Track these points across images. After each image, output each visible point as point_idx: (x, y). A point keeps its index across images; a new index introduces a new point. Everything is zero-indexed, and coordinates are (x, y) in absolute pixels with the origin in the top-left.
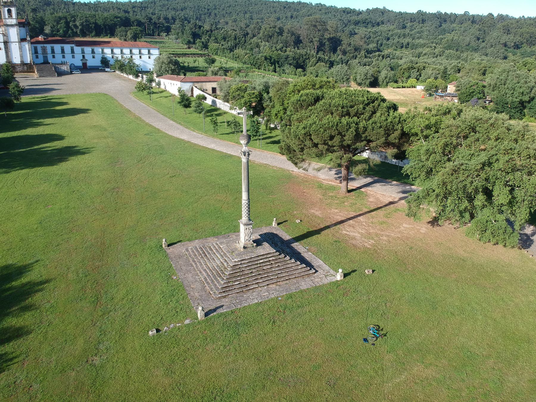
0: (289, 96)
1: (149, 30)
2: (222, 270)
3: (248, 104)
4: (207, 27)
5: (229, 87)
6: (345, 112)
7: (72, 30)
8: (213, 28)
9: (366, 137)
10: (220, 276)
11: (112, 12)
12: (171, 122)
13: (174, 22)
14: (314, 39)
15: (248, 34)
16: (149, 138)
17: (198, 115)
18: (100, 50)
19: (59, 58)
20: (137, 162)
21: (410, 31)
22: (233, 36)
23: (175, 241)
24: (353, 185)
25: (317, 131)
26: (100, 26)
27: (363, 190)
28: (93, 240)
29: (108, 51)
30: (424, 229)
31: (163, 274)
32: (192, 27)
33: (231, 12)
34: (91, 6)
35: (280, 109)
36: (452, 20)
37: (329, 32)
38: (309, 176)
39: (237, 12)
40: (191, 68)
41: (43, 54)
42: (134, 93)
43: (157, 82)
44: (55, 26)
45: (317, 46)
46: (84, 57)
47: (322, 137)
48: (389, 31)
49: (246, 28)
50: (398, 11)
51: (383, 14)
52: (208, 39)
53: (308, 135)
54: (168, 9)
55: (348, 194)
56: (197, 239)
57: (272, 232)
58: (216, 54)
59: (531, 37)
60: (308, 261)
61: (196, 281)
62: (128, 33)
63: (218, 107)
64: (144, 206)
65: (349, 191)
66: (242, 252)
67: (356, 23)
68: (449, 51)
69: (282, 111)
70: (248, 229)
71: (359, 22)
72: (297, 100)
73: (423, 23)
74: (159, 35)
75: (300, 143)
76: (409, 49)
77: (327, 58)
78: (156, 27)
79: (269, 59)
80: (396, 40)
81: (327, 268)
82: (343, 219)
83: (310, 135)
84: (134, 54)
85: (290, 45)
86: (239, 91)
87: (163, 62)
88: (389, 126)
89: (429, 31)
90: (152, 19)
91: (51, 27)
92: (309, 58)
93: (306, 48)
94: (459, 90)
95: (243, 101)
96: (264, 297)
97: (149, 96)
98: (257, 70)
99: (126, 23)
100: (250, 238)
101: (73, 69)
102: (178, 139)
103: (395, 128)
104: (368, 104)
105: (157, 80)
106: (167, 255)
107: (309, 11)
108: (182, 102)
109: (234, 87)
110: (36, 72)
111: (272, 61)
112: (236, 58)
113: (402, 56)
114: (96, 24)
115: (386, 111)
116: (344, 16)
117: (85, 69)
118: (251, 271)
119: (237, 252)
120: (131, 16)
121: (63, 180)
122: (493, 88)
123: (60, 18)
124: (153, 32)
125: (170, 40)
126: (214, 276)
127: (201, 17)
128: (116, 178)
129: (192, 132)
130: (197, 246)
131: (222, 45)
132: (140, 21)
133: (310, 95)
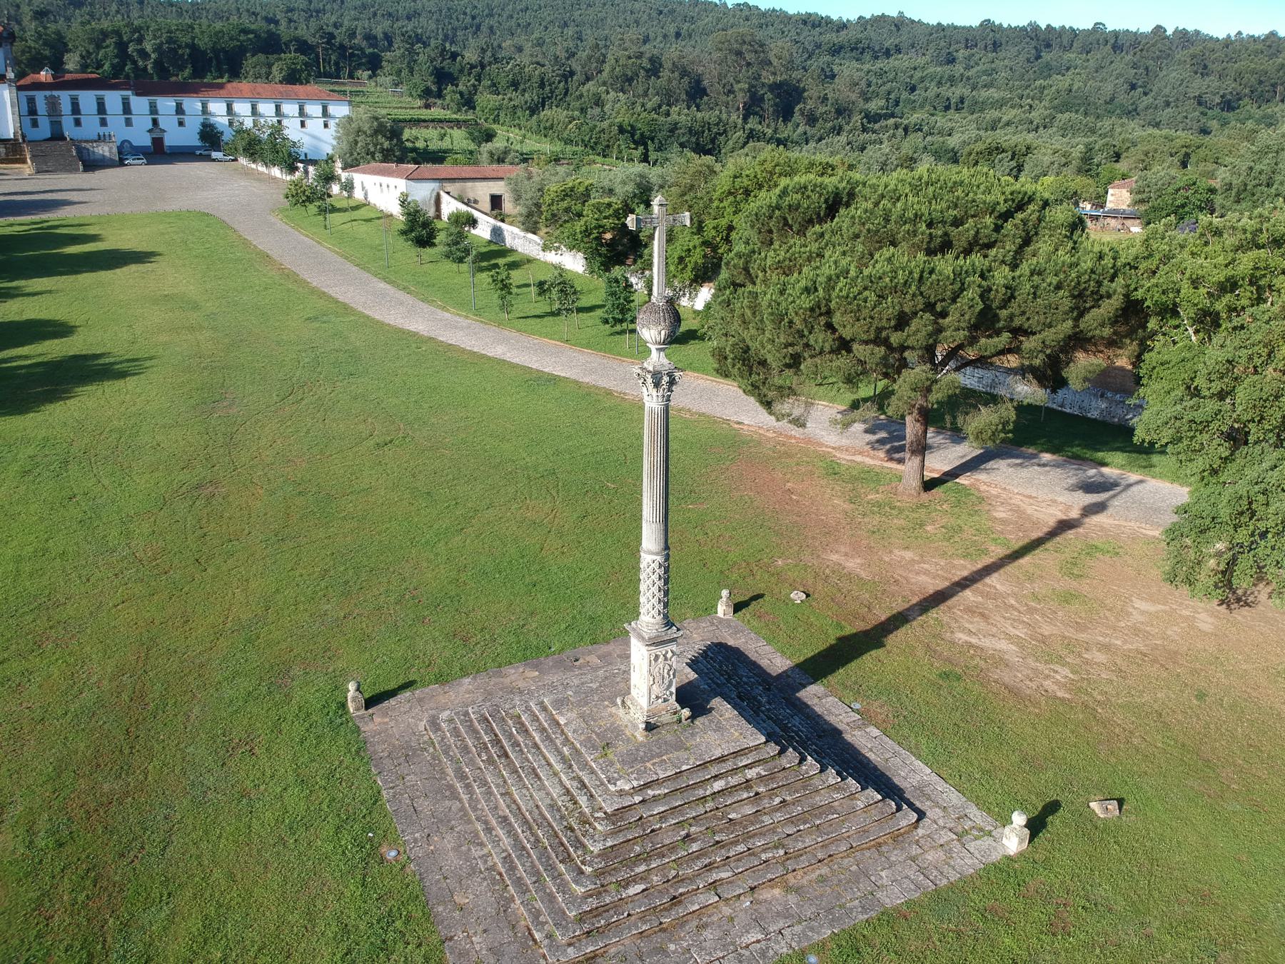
0: (718, 207)
1: (326, 64)
2: (572, 830)
3: (594, 236)
4: (471, 56)
5: (539, 190)
6: (939, 240)
7: (135, 62)
8: (487, 59)
9: (1011, 317)
10: (567, 859)
11: (234, 19)
12: (382, 285)
13: (391, 44)
14: (737, 87)
15: (572, 73)
16: (317, 329)
17: (455, 266)
18: (199, 106)
19: (90, 125)
20: (279, 398)
21: (965, 69)
22: (536, 79)
23: (393, 685)
24: (938, 463)
25: (855, 298)
26: (204, 53)
27: (963, 480)
28: (105, 682)
29: (217, 108)
30: (1203, 616)
31: (346, 839)
32: (433, 55)
33: (529, 24)
34: (184, 8)
35: (691, 244)
36: (1065, 43)
37: (772, 69)
38: (791, 437)
39: (544, 24)
40: (434, 152)
41: (49, 116)
42: (282, 211)
43: (343, 180)
44: (91, 54)
45: (745, 103)
46: (155, 122)
47: (872, 318)
48: (915, 69)
49: (568, 59)
50: (933, 22)
51: (898, 30)
52: (474, 86)
53: (822, 312)
54: (375, 14)
55: (925, 496)
56: (467, 675)
57: (720, 640)
58: (494, 120)
59: (1261, 82)
60: (875, 768)
61: (474, 871)
62: (274, 68)
63: (508, 245)
64: (291, 544)
65: (929, 485)
66: (642, 745)
67: (835, 51)
68: (1067, 115)
69: (698, 250)
70: (662, 658)
71: (841, 48)
72: (770, 206)
73: (995, 51)
74: (351, 76)
75: (791, 339)
76: (965, 113)
77: (769, 132)
78: (345, 57)
79: (628, 132)
80: (933, 90)
81: (954, 797)
82: (941, 585)
83: (829, 313)
84: (287, 117)
85: (677, 101)
86: (569, 199)
87: (359, 131)
88: (1085, 283)
89: (1011, 69)
90: (334, 37)
91: (82, 57)
92: (725, 131)
93: (718, 108)
94: (1142, 201)
95: (579, 226)
96: (747, 953)
97: (321, 218)
98: (599, 159)
99: (270, 45)
100: (667, 689)
101: (126, 153)
102: (402, 331)
103: (1103, 291)
104: (1007, 216)
105: (344, 176)
106: (360, 749)
107: (719, 20)
108: (412, 231)
109: (555, 189)
110: (29, 161)
111: (636, 137)
112: (546, 130)
113: (952, 129)
114: (193, 47)
115: (1066, 236)
116: (805, 33)
117: (158, 152)
118: (683, 833)
119: (621, 747)
120: (283, 30)
121: (45, 460)
122: (1238, 194)
123: (105, 34)
124: (338, 69)
125: (379, 89)
126: (543, 854)
127: (455, 35)
128: (209, 449)
129: (439, 311)
130: (470, 711)
131: (511, 99)
132: (306, 42)
133: (812, 191)
